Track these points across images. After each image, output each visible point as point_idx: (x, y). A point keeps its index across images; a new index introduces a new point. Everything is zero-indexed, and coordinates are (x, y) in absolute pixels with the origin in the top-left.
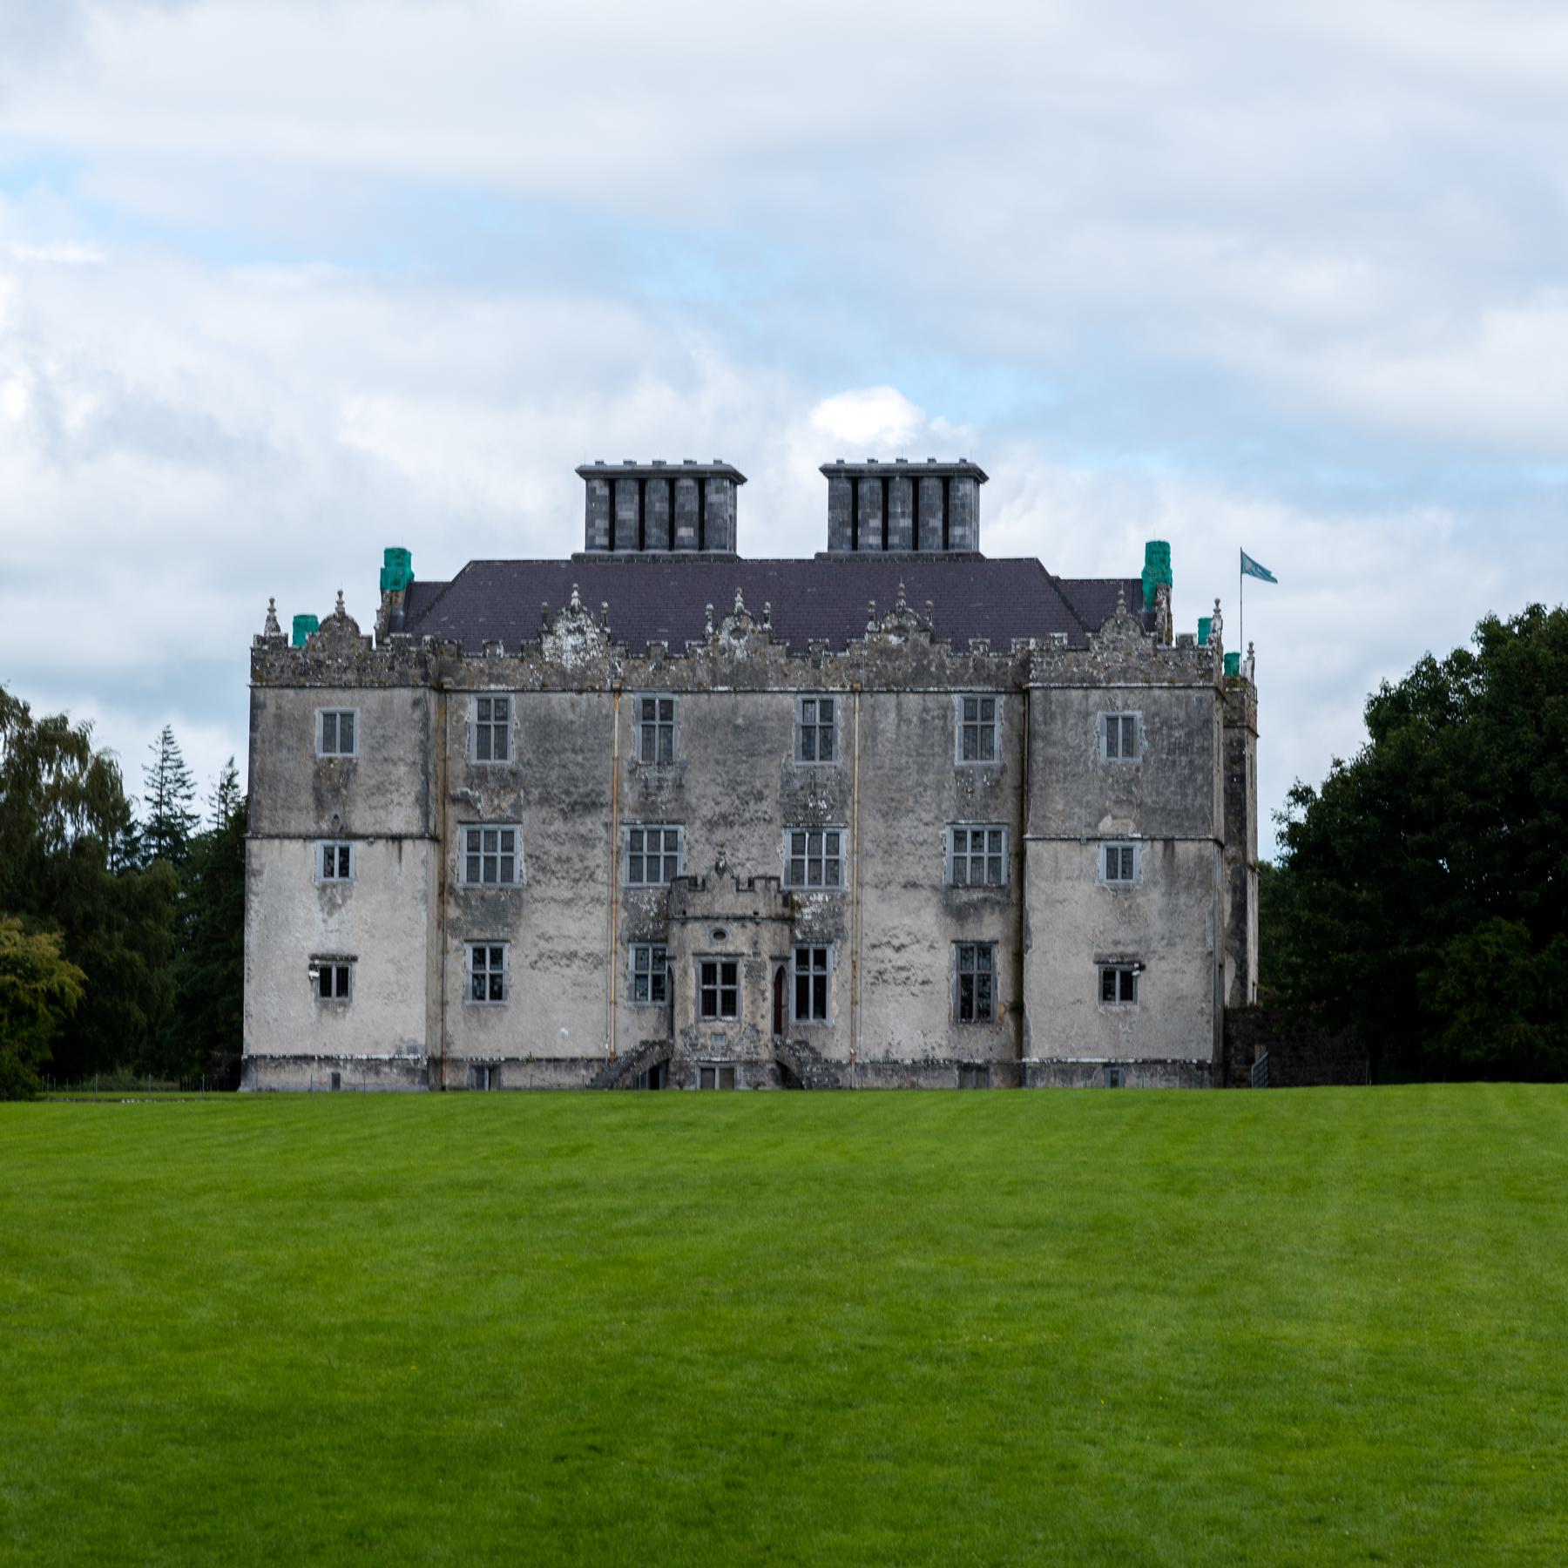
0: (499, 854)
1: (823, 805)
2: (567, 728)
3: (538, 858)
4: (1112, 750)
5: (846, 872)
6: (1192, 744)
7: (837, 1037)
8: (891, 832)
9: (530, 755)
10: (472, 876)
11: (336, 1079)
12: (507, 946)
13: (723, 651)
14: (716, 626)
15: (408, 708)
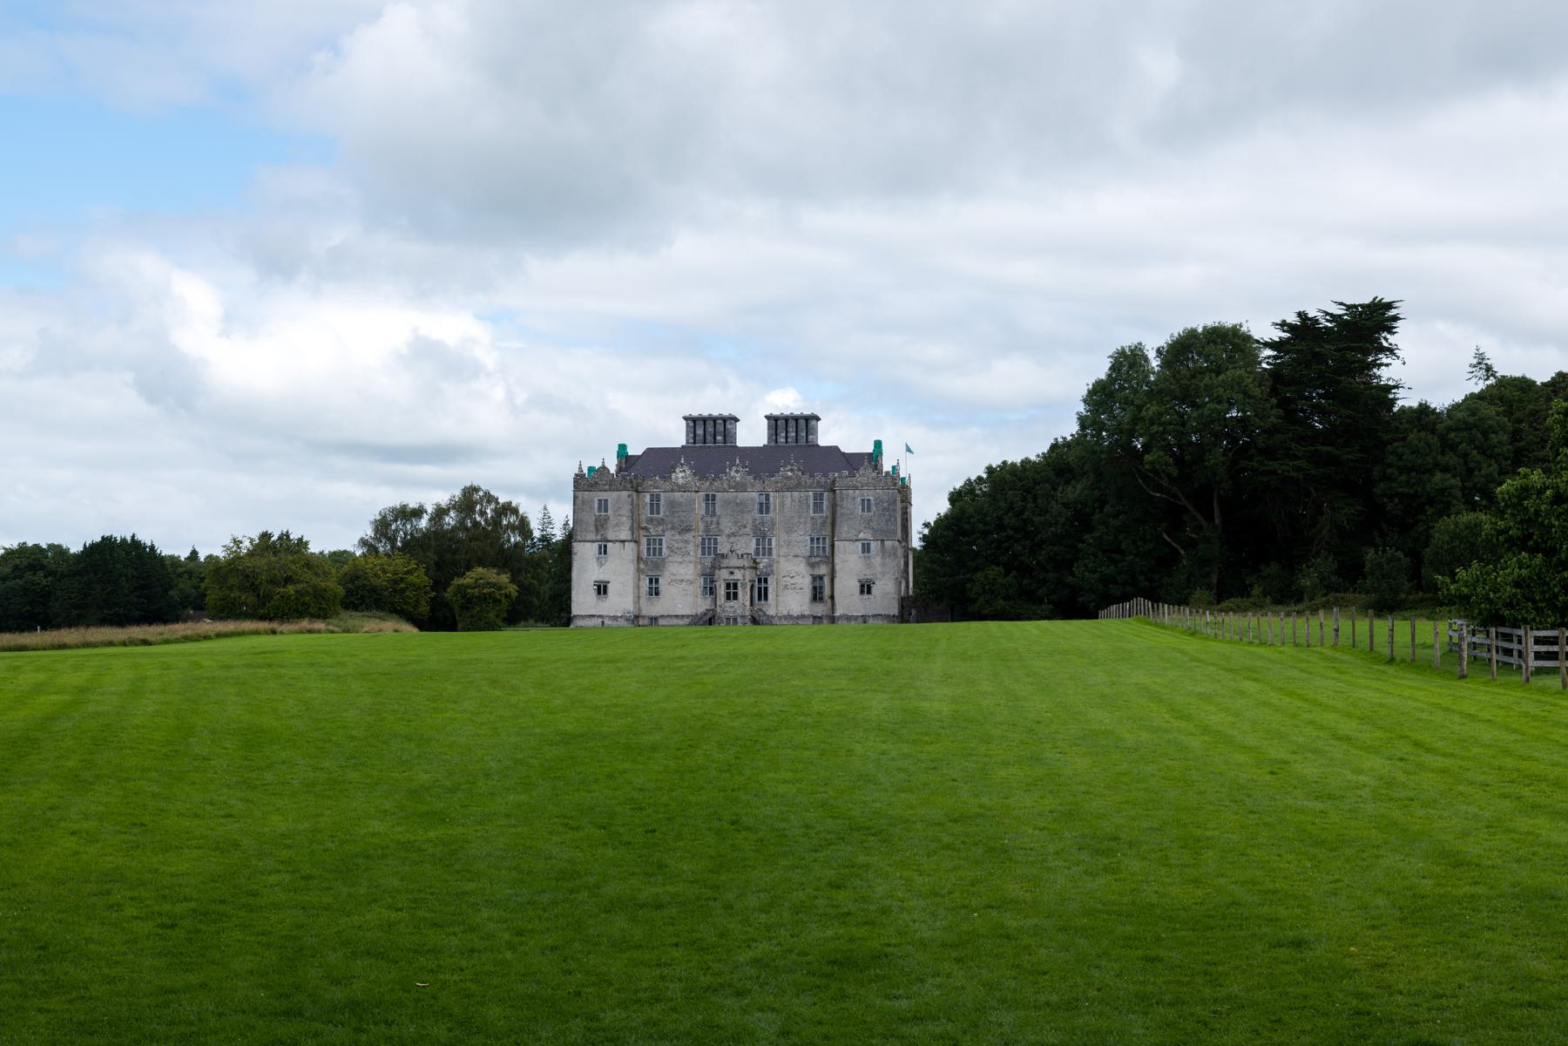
2: (680, 504)
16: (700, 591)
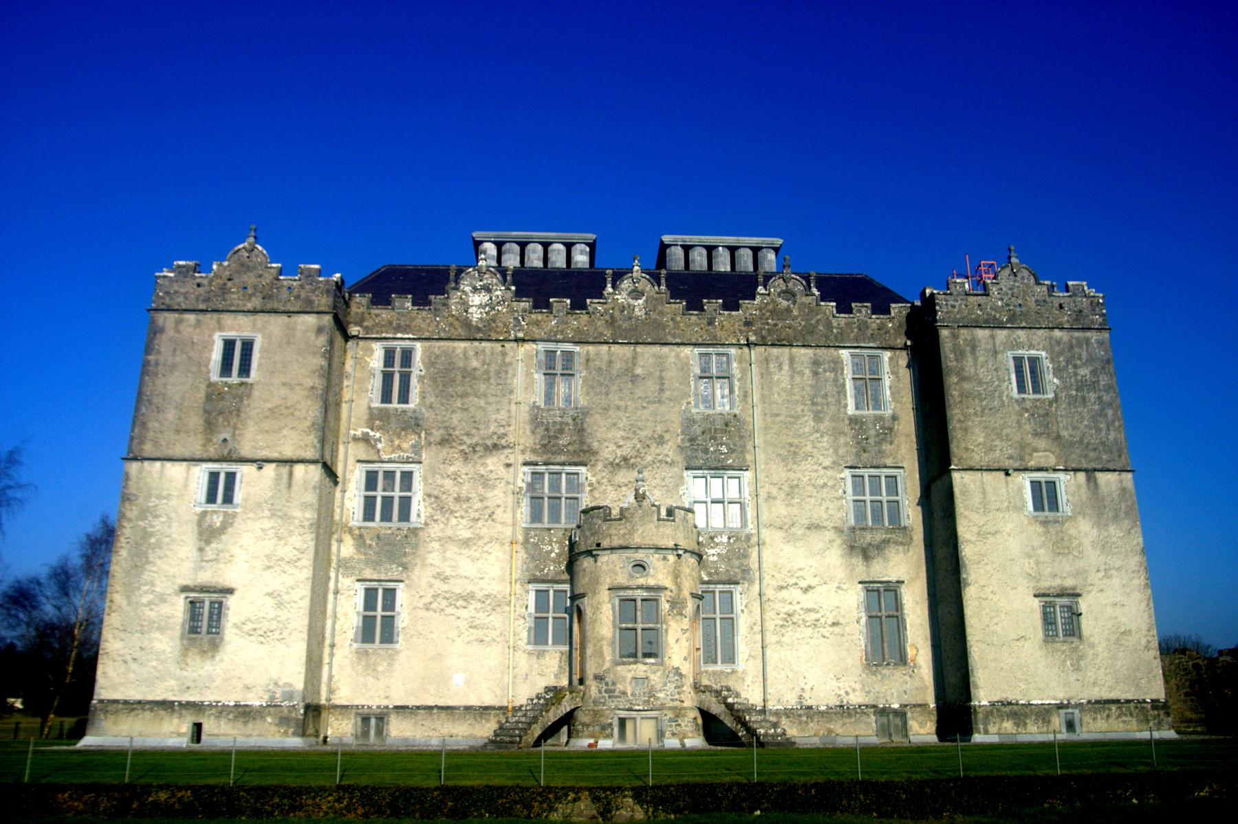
0: (397, 494)
1: (724, 449)
2: (469, 374)
3: (437, 497)
6: (1098, 381)
7: (748, 682)
8: (792, 475)
9: (433, 399)
10: (369, 515)
12: (401, 585)
13: (623, 309)
15: (312, 337)
16: (523, 630)
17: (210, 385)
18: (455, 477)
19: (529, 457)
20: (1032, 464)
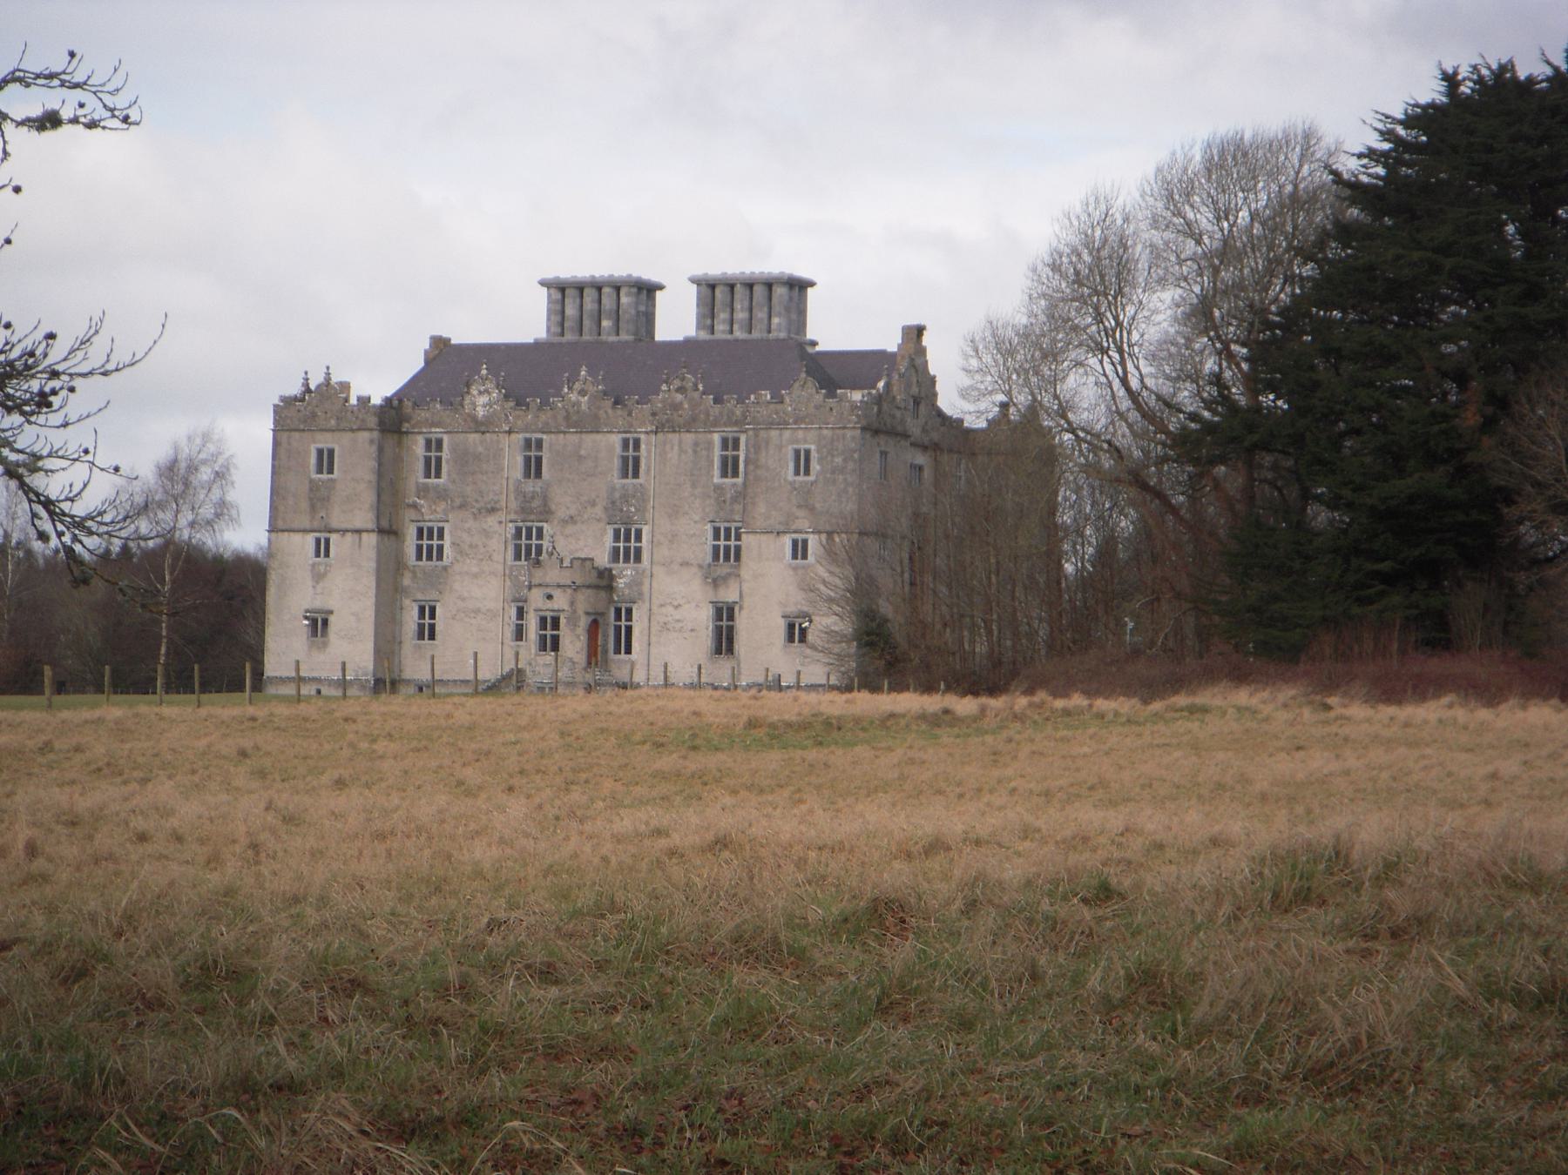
2: (477, 457)
4: (797, 473)
5: (645, 556)
10: (419, 557)
11: (319, 692)
14: (570, 388)
17: (311, 481)
18: (469, 531)
19: (513, 517)
20: (793, 527)
